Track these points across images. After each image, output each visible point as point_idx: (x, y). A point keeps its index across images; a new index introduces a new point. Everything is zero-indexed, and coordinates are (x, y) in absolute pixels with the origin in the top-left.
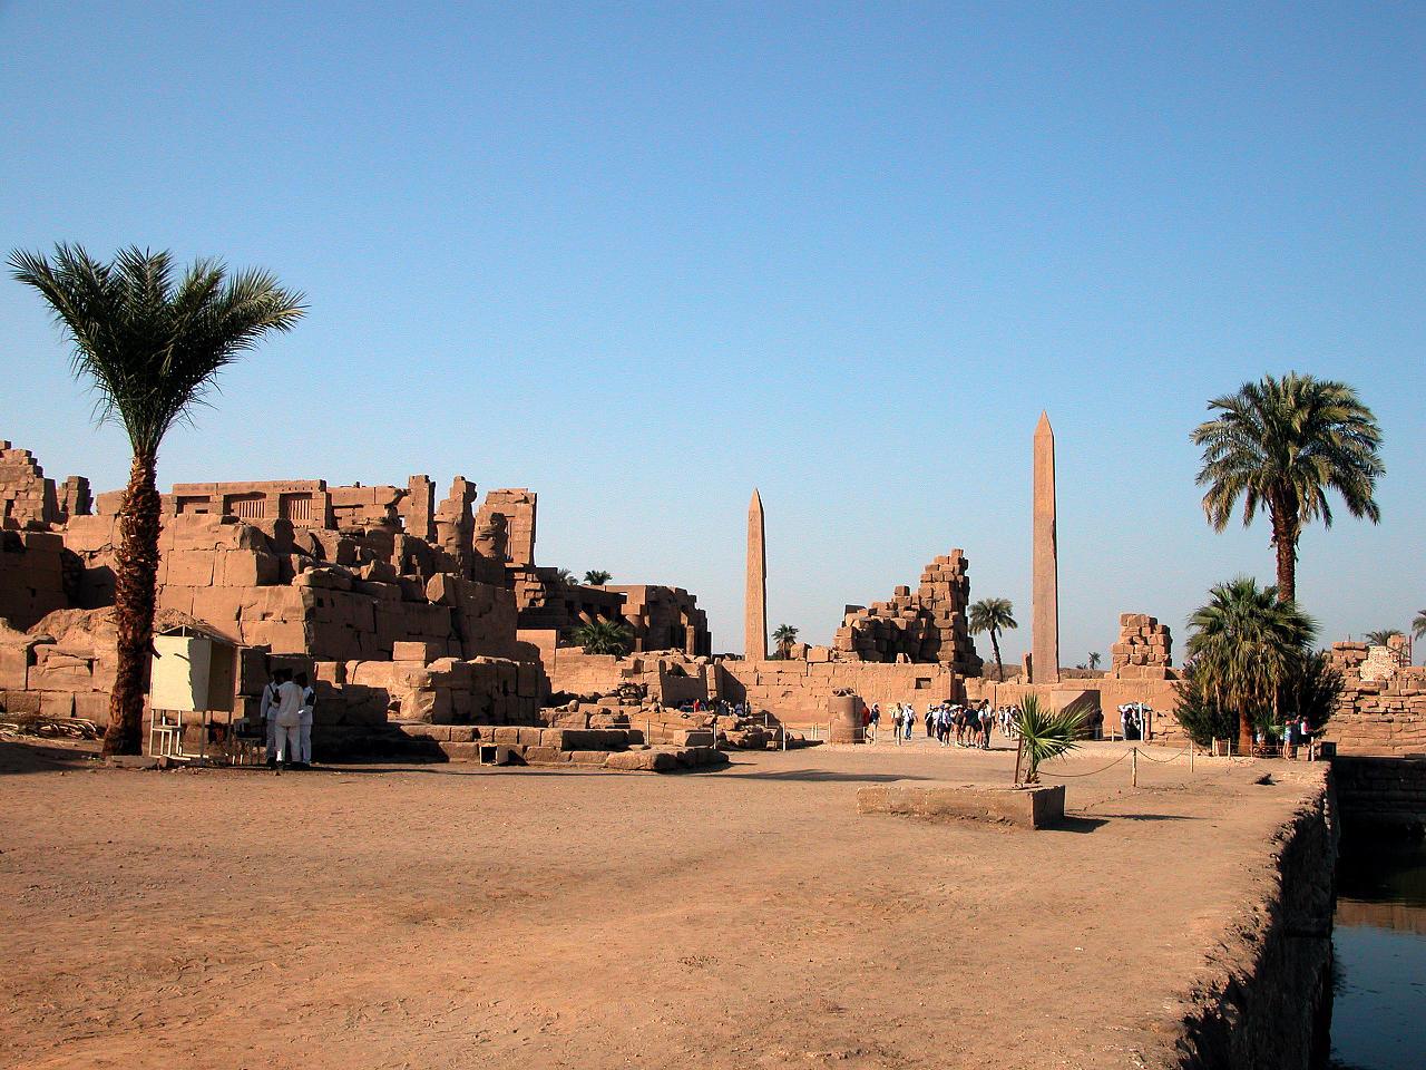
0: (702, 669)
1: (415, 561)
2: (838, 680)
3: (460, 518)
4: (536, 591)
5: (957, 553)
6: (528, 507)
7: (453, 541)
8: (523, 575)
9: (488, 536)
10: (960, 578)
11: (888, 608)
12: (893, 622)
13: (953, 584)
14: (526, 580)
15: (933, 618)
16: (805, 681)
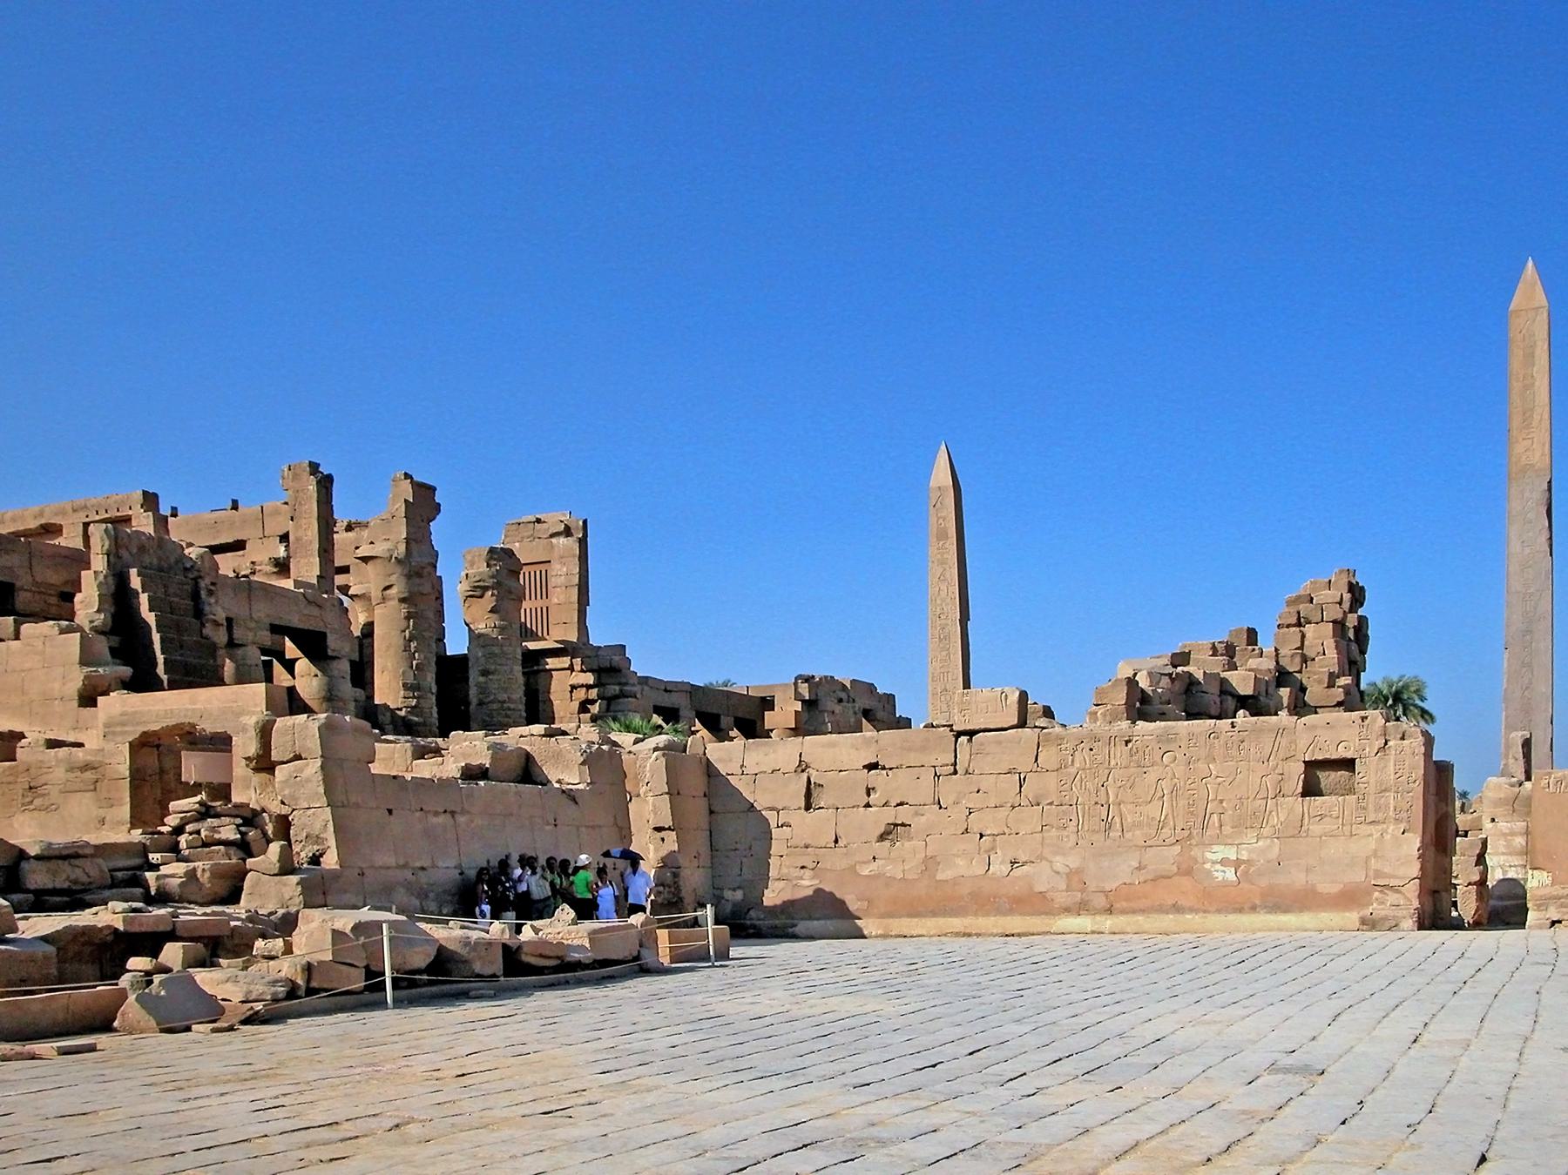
0: (606, 766)
1: (136, 582)
2: (1051, 781)
3: (402, 548)
4: (589, 687)
5: (1344, 575)
6: (569, 544)
7: (394, 591)
8: (565, 662)
9: (485, 589)
10: (1352, 620)
11: (1215, 653)
12: (1224, 682)
13: (1339, 625)
14: (571, 668)
15: (1303, 690)
16: (950, 788)
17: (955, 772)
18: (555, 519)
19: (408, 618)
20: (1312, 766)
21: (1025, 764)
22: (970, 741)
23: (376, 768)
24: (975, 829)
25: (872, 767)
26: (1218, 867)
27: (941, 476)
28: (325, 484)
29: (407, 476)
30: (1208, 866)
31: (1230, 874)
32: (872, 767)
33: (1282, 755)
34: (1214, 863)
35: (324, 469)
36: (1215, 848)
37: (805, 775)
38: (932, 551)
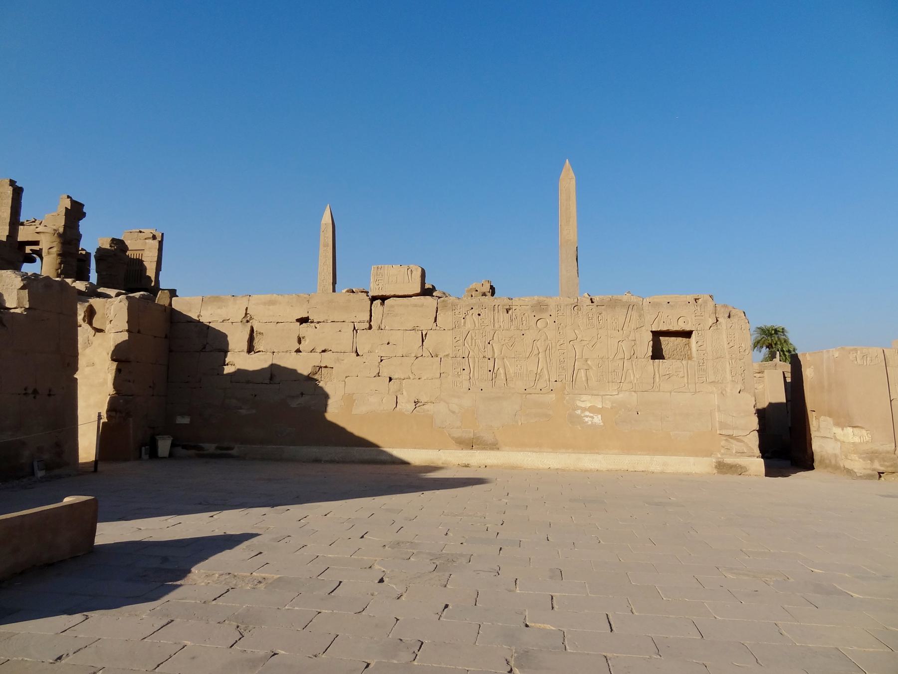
16: (365, 341)
17: (370, 328)
18: (148, 232)
19: (60, 264)
20: (657, 335)
21: (426, 323)
22: (383, 304)
23: (228, 370)
24: (385, 374)
25: (303, 320)
26: (587, 413)
27: (326, 219)
28: (18, 192)
29: (68, 197)
30: (579, 412)
31: (598, 419)
32: (303, 320)
33: (633, 326)
34: (584, 410)
35: (18, 184)
36: (584, 397)
37: (249, 325)
38: (321, 251)
